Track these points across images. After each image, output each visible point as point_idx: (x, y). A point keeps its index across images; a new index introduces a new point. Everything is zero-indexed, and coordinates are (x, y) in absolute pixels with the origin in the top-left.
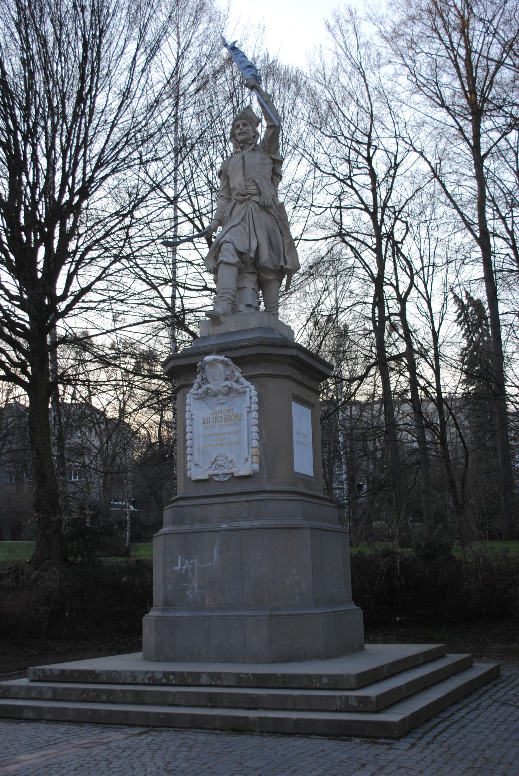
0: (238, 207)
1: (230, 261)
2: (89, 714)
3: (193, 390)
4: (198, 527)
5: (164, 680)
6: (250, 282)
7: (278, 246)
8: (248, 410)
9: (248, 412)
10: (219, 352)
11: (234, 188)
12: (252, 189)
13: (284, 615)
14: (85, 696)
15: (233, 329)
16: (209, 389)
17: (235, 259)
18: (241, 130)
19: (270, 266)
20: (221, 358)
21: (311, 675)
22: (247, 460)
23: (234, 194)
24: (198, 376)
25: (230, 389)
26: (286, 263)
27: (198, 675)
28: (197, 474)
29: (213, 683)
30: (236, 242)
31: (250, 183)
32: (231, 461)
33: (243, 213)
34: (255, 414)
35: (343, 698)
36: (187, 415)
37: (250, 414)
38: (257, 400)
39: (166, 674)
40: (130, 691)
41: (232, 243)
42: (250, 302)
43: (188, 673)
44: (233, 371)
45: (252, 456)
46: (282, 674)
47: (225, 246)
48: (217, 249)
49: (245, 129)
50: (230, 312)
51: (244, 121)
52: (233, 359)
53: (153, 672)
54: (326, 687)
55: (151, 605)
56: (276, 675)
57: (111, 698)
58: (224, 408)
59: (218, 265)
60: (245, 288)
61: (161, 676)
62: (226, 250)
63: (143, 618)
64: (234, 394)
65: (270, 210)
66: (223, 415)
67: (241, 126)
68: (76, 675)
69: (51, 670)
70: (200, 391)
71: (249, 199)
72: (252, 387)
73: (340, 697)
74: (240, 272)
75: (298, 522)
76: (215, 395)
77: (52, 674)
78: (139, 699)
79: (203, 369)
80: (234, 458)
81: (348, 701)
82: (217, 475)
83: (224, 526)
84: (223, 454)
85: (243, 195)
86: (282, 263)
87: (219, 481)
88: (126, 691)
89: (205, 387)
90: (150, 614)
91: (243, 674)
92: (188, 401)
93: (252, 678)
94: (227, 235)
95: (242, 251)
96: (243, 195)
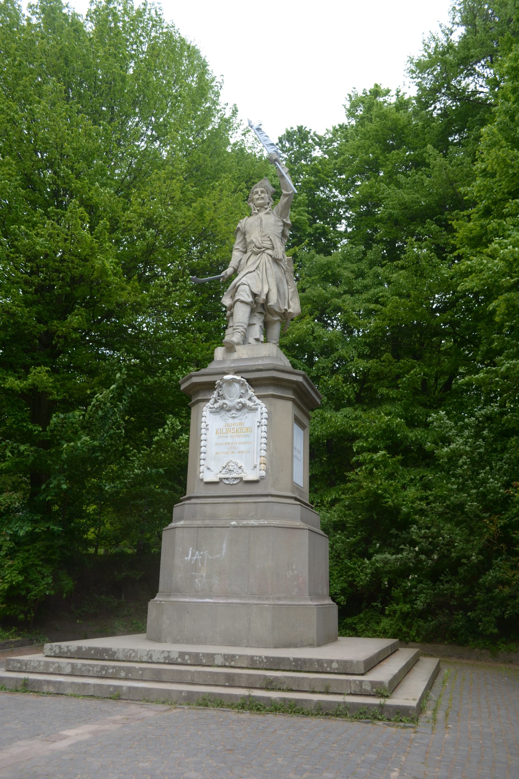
0: (253, 258)
1: (245, 300)
2: (111, 689)
3: (209, 404)
4: (207, 522)
5: (179, 660)
6: (258, 322)
7: (284, 293)
8: (258, 424)
9: (258, 426)
10: (237, 373)
11: (252, 242)
12: (267, 244)
13: (285, 605)
14: (104, 672)
15: (245, 356)
16: (224, 404)
17: (250, 299)
18: (260, 195)
19: (277, 310)
20: (238, 378)
21: (321, 660)
22: (255, 467)
23: (251, 247)
24: (215, 392)
25: (244, 406)
26: (289, 307)
27: (212, 656)
28: (208, 477)
29: (227, 664)
30: (251, 285)
31: (266, 238)
32: (240, 468)
33: (258, 262)
34: (264, 428)
35: (357, 682)
36: (203, 425)
37: (260, 428)
38: (267, 416)
39: (182, 655)
40: (149, 669)
41: (249, 286)
42: (258, 337)
43: (203, 654)
44: (247, 390)
45: (261, 464)
46: (294, 658)
47: (242, 287)
48: (234, 290)
49: (263, 195)
50: (242, 342)
51: (262, 189)
52: (248, 380)
53: (169, 652)
54: (336, 671)
55: (157, 591)
56: (288, 659)
57: (130, 675)
58: (236, 421)
59: (235, 303)
60: (254, 324)
61: (177, 656)
62: (243, 291)
63: (151, 605)
64: (245, 410)
65: (281, 263)
66: (235, 427)
67: (259, 193)
68: (92, 652)
69: (68, 647)
70: (216, 405)
71: (263, 252)
72: (263, 405)
73: (355, 681)
74: (252, 311)
75: (298, 524)
76: (229, 411)
77: (69, 651)
78: (157, 677)
79: (220, 386)
80: (243, 465)
81: (361, 686)
82: (227, 479)
83: (233, 523)
84: (234, 461)
85: (259, 248)
86: (286, 307)
87: (229, 484)
88: (146, 669)
89: (221, 402)
90: (156, 598)
91: (257, 656)
92: (204, 413)
93: (265, 660)
94: (244, 278)
95: (256, 292)
96: (259, 248)
